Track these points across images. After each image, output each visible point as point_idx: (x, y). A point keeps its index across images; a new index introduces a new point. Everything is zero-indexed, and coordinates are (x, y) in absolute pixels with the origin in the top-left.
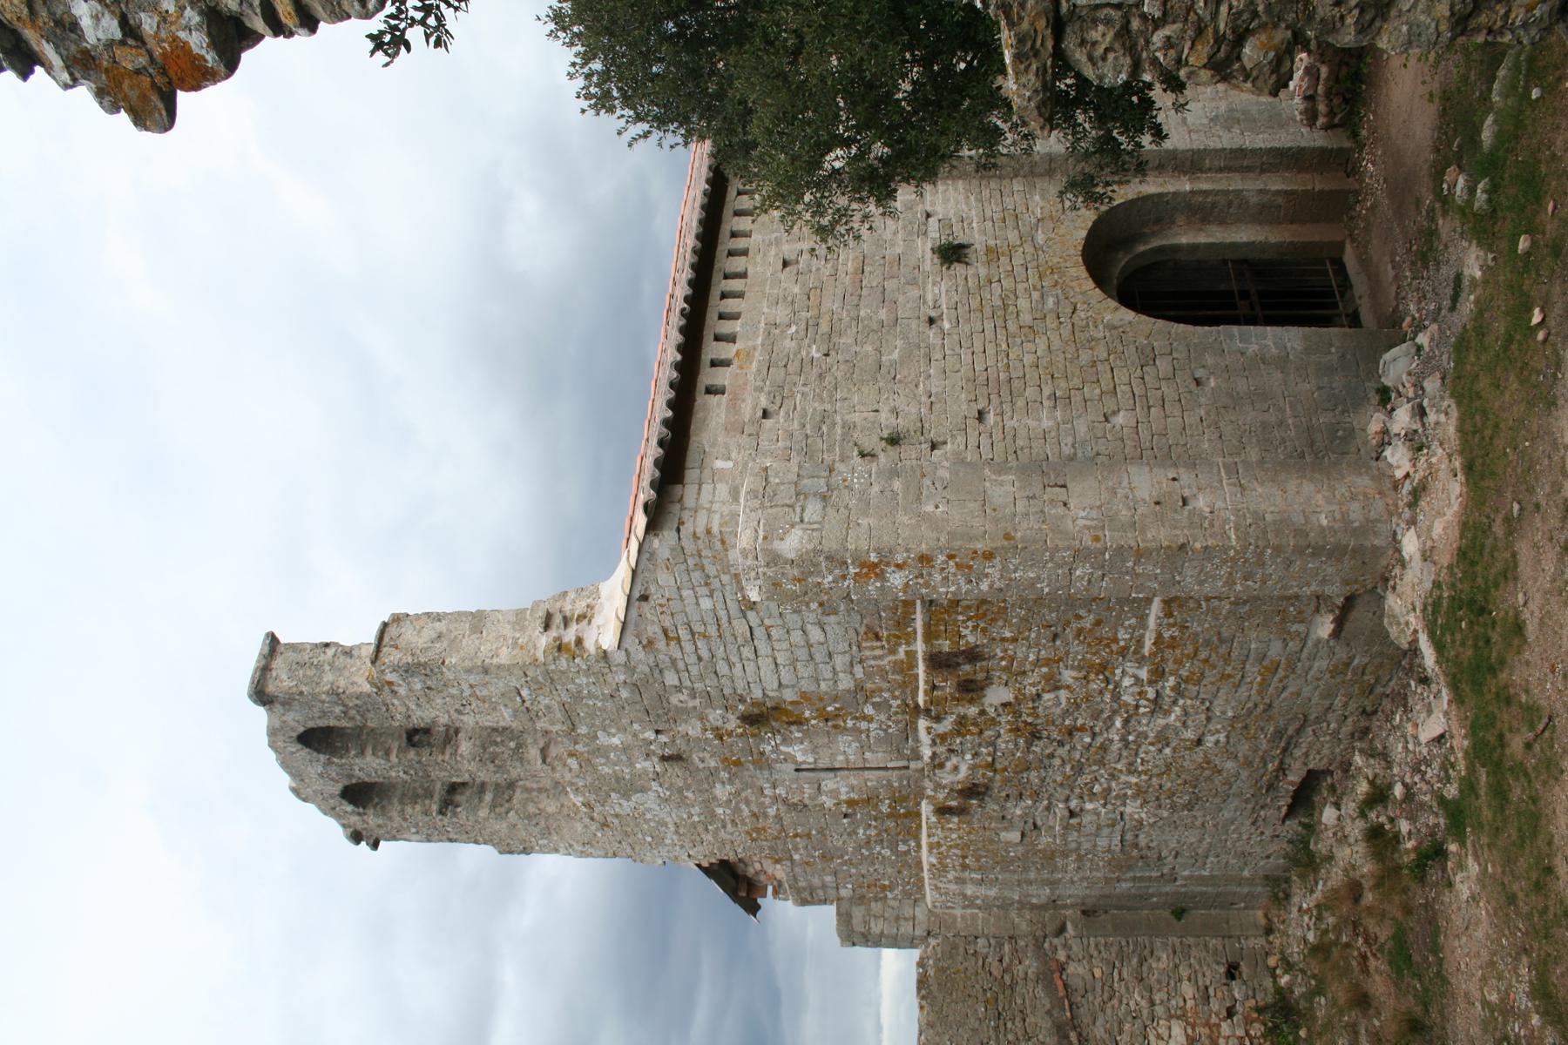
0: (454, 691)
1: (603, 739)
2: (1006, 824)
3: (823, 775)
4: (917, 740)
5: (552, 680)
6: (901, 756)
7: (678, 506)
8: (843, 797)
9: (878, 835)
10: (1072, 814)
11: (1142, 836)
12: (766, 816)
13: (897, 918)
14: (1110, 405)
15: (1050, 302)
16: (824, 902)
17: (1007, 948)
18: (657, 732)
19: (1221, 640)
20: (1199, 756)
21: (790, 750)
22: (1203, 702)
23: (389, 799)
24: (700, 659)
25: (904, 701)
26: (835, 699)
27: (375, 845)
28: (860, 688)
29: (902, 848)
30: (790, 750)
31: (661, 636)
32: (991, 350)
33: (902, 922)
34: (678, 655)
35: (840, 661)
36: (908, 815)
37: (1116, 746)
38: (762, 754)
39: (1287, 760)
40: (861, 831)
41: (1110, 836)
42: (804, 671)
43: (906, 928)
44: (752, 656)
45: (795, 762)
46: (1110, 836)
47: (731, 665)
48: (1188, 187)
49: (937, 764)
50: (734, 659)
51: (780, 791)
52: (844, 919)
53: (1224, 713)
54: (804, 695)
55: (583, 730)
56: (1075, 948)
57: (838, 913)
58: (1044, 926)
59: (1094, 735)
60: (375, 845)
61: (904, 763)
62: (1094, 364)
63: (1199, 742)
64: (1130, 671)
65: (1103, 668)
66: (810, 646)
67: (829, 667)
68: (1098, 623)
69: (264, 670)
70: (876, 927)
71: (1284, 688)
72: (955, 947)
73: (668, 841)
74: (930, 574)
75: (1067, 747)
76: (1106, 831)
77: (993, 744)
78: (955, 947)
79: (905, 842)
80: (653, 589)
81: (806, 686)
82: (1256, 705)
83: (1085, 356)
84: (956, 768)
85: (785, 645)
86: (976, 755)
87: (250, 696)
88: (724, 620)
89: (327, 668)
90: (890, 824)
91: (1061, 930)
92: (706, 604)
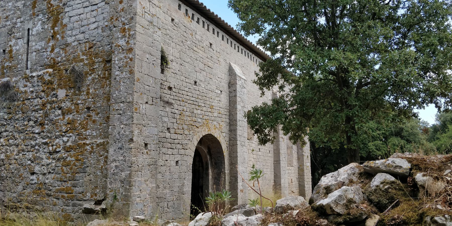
4: (40, 71)
6: (33, 65)
8: (14, 48)
14: (172, 131)
15: (199, 120)
19: (84, 169)
22: (53, 170)
25: (60, 62)
32: (188, 97)
35: (81, 36)
37: (33, 143)
38: (38, 15)
42: (76, 25)
44: (84, 6)
45: (33, 28)
48: (226, 172)
49: (27, 78)
51: (19, 25)
53: (47, 179)
54: (66, 25)
61: (29, 66)
62: (183, 129)
63: (33, 174)
64: (71, 139)
67: (78, 33)
68: (94, 121)
71: (58, 199)
75: (34, 125)
77: (37, 97)
81: (70, 26)
83: (185, 127)
84: (26, 86)
85: (88, 17)
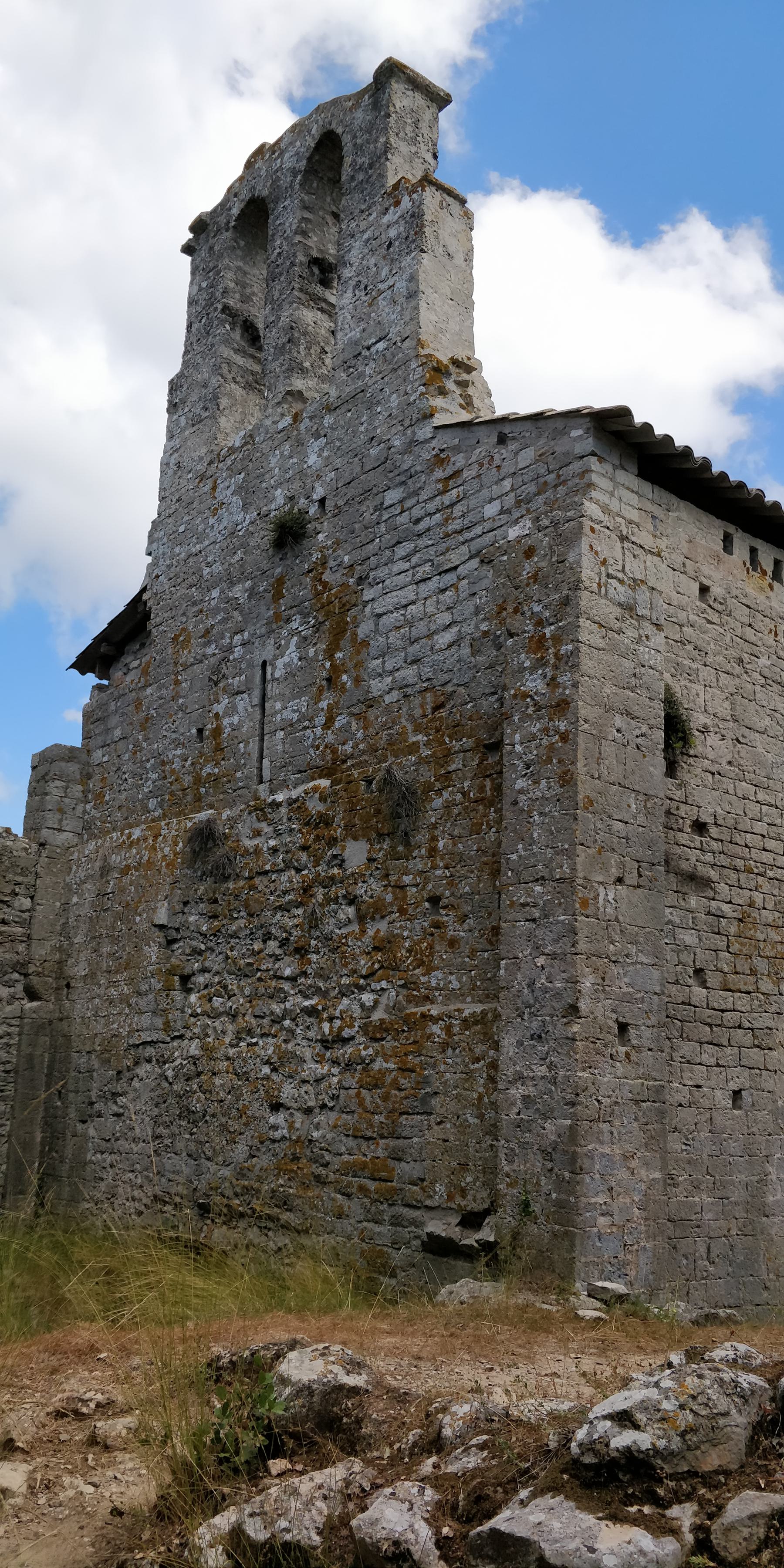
0: (384, 273)
1: (316, 445)
2: (179, 907)
3: (257, 693)
5: (395, 370)
6: (277, 769)
7: (617, 463)
9: (173, 771)
10: (185, 979)
11: (148, 1067)
12: (207, 644)
13: (61, 811)
14: (713, 980)
16: (87, 736)
17: (19, 930)
18: (322, 502)
20: (258, 1109)
21: (292, 648)
22: (334, 1097)
23: (243, 258)
24: (418, 521)
26: (357, 681)
27: (188, 249)
28: (371, 703)
29: (152, 803)
30: (292, 648)
31: (449, 471)
33: (58, 816)
34: (423, 496)
35: (409, 674)
36: (198, 799)
37: (277, 1008)
39: (242, 1224)
40: (179, 752)
41: (153, 1028)
42: (394, 638)
43: (52, 819)
44: (418, 577)
46: (153, 1028)
47: (407, 558)
49: (262, 810)
50: (415, 560)
52: (70, 754)
53: (317, 1127)
54: (365, 644)
55: (328, 420)
56: (9, 1008)
57: (72, 749)
58: (38, 974)
59: (292, 979)
60: (188, 249)
62: (753, 972)
63: (276, 1107)
65: (392, 967)
66: (429, 636)
67: (401, 663)
68: (453, 943)
69: (416, 83)
70: (55, 788)
71: (348, 1196)
72: (24, 872)
73: (177, 550)
74: (539, 719)
75: (278, 951)
76: (159, 1022)
78: (24, 872)
79: (161, 805)
80: (513, 446)
82: (326, 1165)
84: (257, 833)
86: (274, 850)
87: (389, 60)
88: (468, 535)
89: (414, 149)
90: (187, 780)
91: (32, 994)
92: (491, 510)
